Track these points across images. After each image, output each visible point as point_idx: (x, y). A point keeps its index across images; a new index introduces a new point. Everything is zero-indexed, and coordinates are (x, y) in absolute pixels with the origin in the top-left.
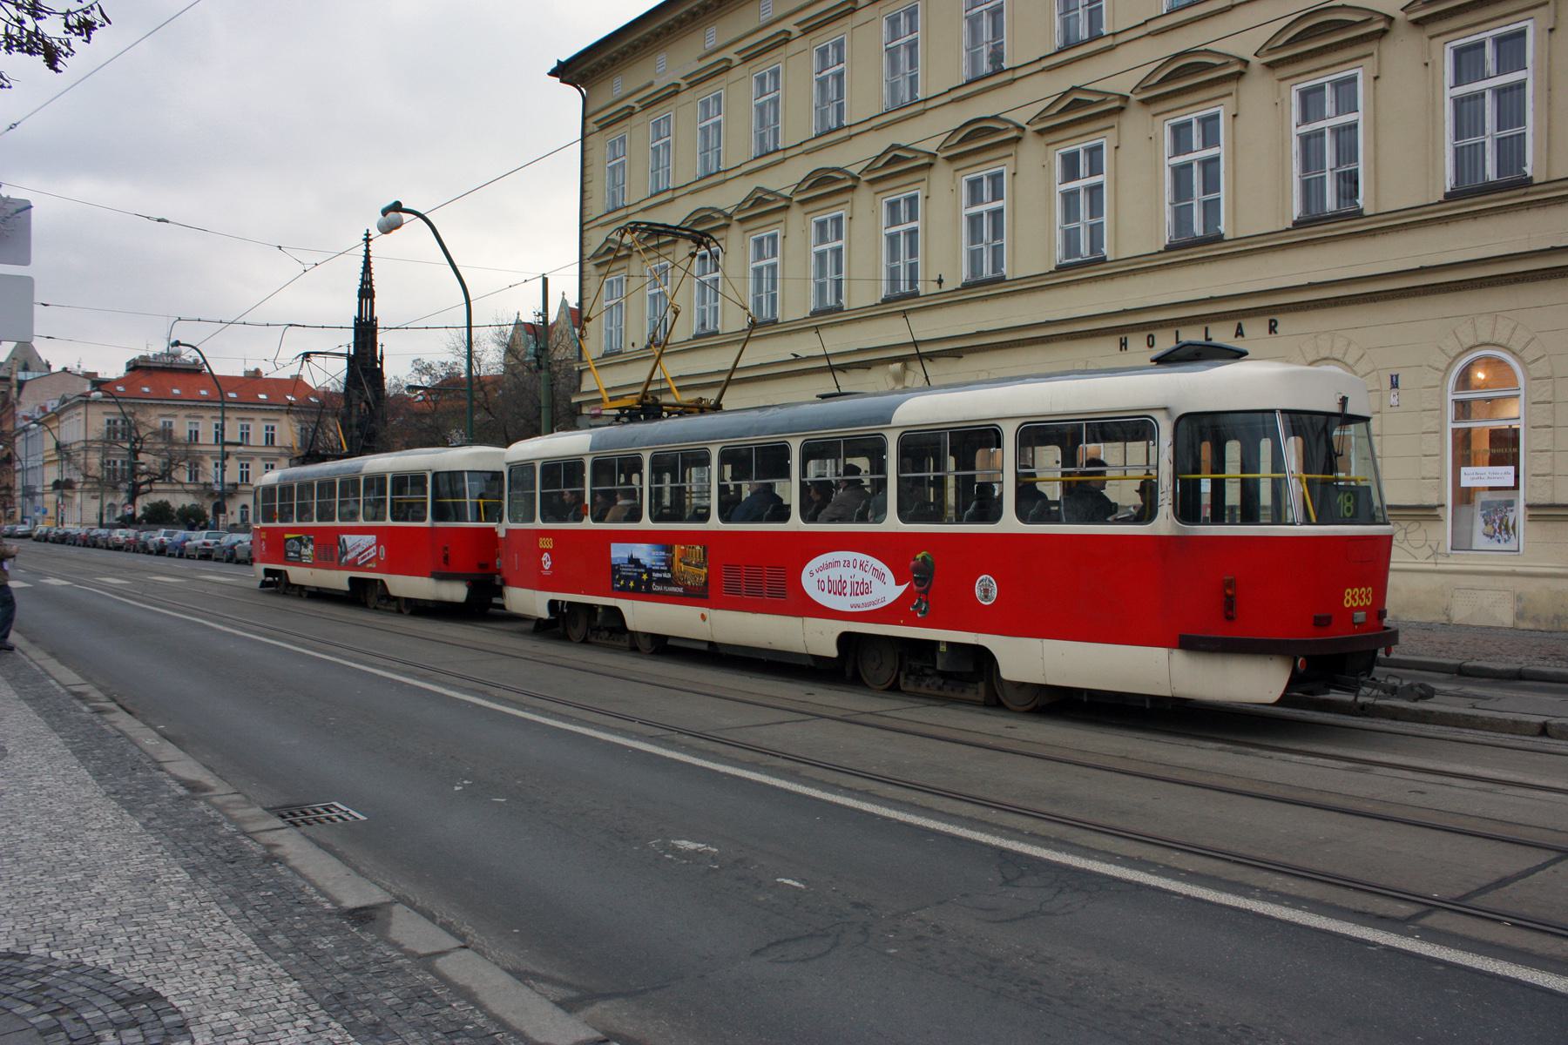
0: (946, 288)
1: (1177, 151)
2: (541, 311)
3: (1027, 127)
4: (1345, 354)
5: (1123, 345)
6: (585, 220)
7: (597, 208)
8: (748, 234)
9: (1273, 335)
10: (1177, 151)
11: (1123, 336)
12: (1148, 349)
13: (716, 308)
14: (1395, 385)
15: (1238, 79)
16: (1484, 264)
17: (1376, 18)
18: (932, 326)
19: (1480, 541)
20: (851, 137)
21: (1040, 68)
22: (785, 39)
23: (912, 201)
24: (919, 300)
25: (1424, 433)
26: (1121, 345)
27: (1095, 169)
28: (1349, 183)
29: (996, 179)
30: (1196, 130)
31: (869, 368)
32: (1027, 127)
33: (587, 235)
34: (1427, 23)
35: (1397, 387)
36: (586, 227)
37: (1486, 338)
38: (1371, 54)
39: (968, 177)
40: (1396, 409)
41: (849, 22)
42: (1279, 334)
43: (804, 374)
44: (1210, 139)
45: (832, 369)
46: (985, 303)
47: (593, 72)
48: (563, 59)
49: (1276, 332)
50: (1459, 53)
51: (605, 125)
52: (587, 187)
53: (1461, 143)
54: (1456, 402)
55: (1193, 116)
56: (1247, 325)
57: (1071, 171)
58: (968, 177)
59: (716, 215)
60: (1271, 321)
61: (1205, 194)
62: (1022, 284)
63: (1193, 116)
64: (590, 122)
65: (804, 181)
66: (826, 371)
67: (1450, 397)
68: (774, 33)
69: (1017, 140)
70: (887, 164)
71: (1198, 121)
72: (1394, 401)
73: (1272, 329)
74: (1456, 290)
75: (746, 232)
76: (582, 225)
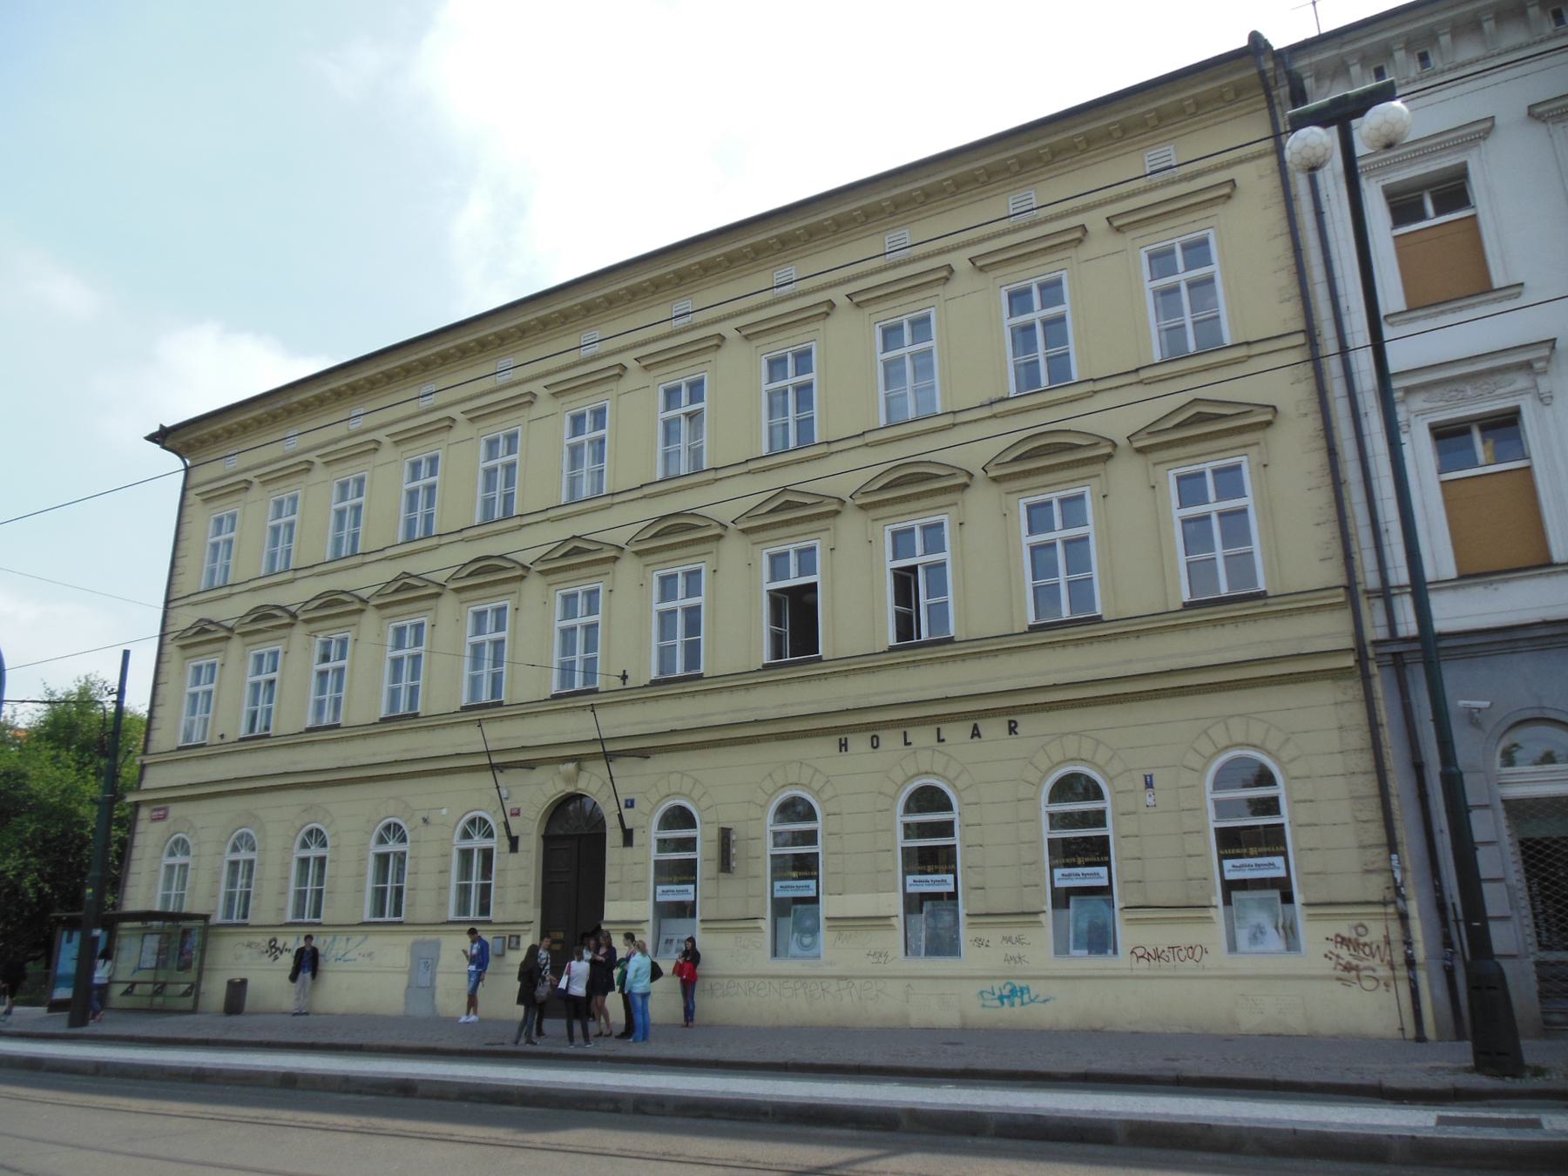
0: (630, 684)
1: (663, 598)
2: (116, 688)
3: (626, 547)
4: (1049, 757)
5: (843, 746)
6: (172, 597)
7: (191, 581)
8: (465, 605)
9: (1013, 735)
10: (663, 598)
11: (843, 737)
12: (872, 750)
13: (206, 720)
14: (1149, 784)
15: (963, 490)
16: (1271, 663)
17: (1103, 443)
18: (621, 722)
19: (794, 948)
20: (230, 595)
21: (247, 589)
22: (308, 467)
23: (419, 628)
24: (501, 709)
25: (1185, 833)
26: (841, 745)
27: (592, 609)
28: (693, 651)
29: (592, 595)
30: (681, 581)
31: (534, 768)
32: (626, 547)
33: (172, 613)
34: (870, 508)
35: (1152, 787)
36: (172, 605)
37: (1239, 738)
38: (712, 552)
39: (659, 572)
40: (1151, 810)
41: (526, 414)
42: (1020, 735)
43: (719, 746)
44: (693, 590)
45: (493, 767)
46: (1113, 644)
47: (203, 443)
48: (168, 424)
49: (1016, 733)
50: (896, 535)
51: (208, 498)
52: (179, 562)
53: (1040, 582)
54: (659, 840)
55: (917, 523)
56: (984, 726)
57: (667, 590)
58: (659, 572)
59: (212, 628)
60: (1010, 722)
61: (586, 652)
62: (723, 682)
63: (917, 523)
64: (191, 494)
65: (247, 615)
66: (599, 759)
67: (653, 836)
68: (436, 419)
69: (719, 537)
70: (397, 591)
71: (683, 573)
72: (1150, 801)
73: (1012, 729)
74: (1237, 689)
75: (186, 658)
76: (167, 602)
